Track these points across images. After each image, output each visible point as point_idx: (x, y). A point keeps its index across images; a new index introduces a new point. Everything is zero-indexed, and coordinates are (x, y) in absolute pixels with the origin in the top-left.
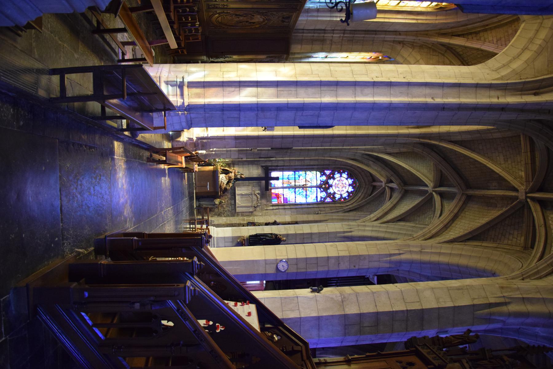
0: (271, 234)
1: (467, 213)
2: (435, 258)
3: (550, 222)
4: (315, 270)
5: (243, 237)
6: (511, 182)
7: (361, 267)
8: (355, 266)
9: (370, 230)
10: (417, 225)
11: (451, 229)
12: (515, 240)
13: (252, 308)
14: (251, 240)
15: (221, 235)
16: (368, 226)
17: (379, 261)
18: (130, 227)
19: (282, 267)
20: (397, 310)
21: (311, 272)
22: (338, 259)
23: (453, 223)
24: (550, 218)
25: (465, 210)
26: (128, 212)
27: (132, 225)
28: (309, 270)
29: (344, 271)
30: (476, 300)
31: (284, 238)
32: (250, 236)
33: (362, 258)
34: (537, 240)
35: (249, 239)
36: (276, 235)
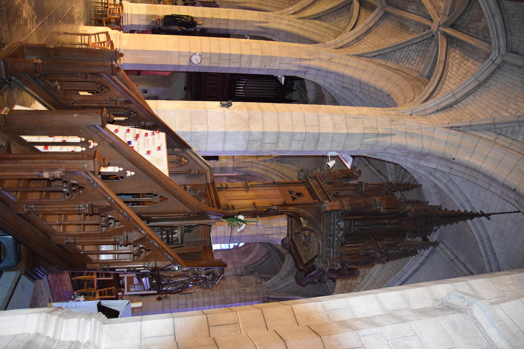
0: (187, 16)
1: (380, 29)
2: (341, 70)
3: (450, 59)
4: (227, 66)
5: (159, 17)
6: (429, 11)
7: (271, 68)
8: (265, 66)
9: (285, 24)
10: (332, 27)
11: (362, 42)
12: (416, 66)
13: (161, 138)
14: (166, 20)
15: (135, 12)
16: (285, 19)
17: (289, 64)
18: (31, 28)
19: (196, 60)
20: (297, 131)
21: (222, 67)
22: (251, 57)
23: (365, 36)
24: (451, 56)
25: (379, 26)
26: (28, 12)
27: (35, 25)
28: (221, 65)
29: (255, 69)
30: (367, 129)
31: (200, 22)
32: (166, 17)
33: (273, 59)
34: (434, 75)
35: (165, 19)
36: (192, 18)
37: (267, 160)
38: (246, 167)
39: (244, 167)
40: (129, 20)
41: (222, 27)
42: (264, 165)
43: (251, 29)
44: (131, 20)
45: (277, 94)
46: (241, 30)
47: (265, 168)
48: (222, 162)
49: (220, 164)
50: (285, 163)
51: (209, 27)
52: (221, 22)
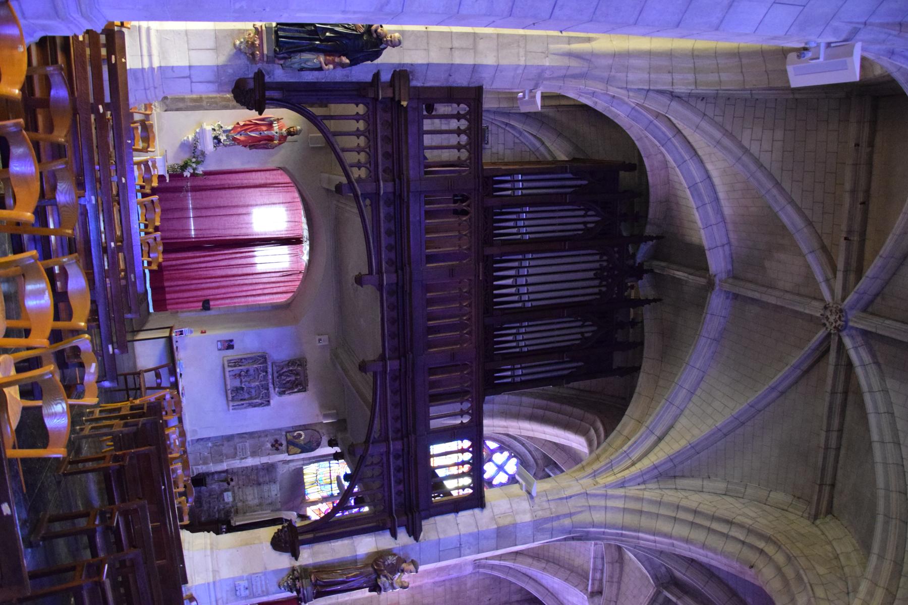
37: (630, 480)
38: (570, 515)
40: (155, 52)
41: (459, 59)
42: (625, 497)
43: (547, 63)
44: (163, 53)
45: (604, 289)
46: (517, 67)
47: (631, 505)
48: (497, 511)
49: (493, 518)
50: (683, 476)
52: (456, 44)
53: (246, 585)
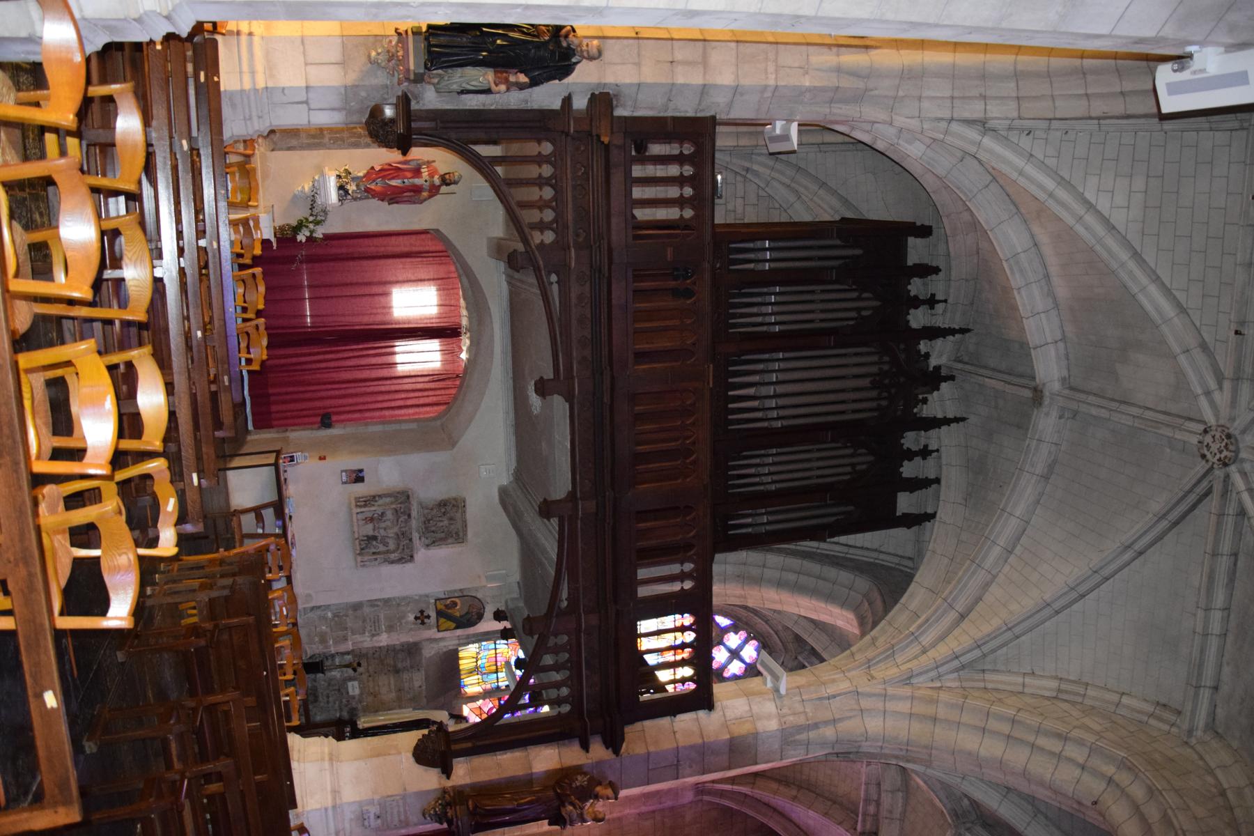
14: (433, 41)
39: (826, 723)
40: (260, 67)
43: (807, 82)
44: (270, 68)
45: (884, 403)
47: (920, 708)
48: (730, 714)
51: (628, 80)
53: (378, 813)
